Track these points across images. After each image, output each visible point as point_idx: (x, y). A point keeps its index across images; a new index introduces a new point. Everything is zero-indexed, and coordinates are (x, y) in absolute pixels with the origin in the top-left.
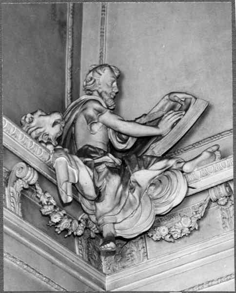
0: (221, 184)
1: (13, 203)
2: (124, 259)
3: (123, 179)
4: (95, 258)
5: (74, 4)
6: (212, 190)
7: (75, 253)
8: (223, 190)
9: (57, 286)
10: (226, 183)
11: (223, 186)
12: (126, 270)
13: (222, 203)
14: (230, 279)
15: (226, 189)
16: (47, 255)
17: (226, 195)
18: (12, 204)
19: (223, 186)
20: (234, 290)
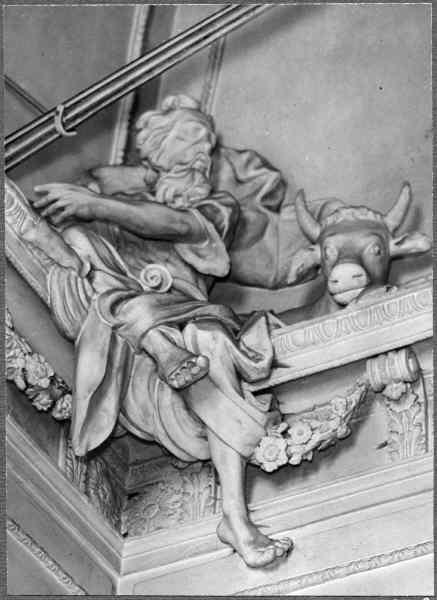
0: (397, 350)
1: (71, 460)
2: (163, 513)
3: (129, 156)
4: (105, 497)
5: (152, 9)
6: (375, 363)
7: (56, 465)
8: (400, 365)
9: (77, 588)
10: (409, 349)
11: (403, 354)
12: (163, 533)
13: (395, 395)
14: (423, 554)
15: (407, 362)
16: (59, 517)
17: (409, 378)
18: (69, 462)
19: (403, 354)
20: (432, 592)
